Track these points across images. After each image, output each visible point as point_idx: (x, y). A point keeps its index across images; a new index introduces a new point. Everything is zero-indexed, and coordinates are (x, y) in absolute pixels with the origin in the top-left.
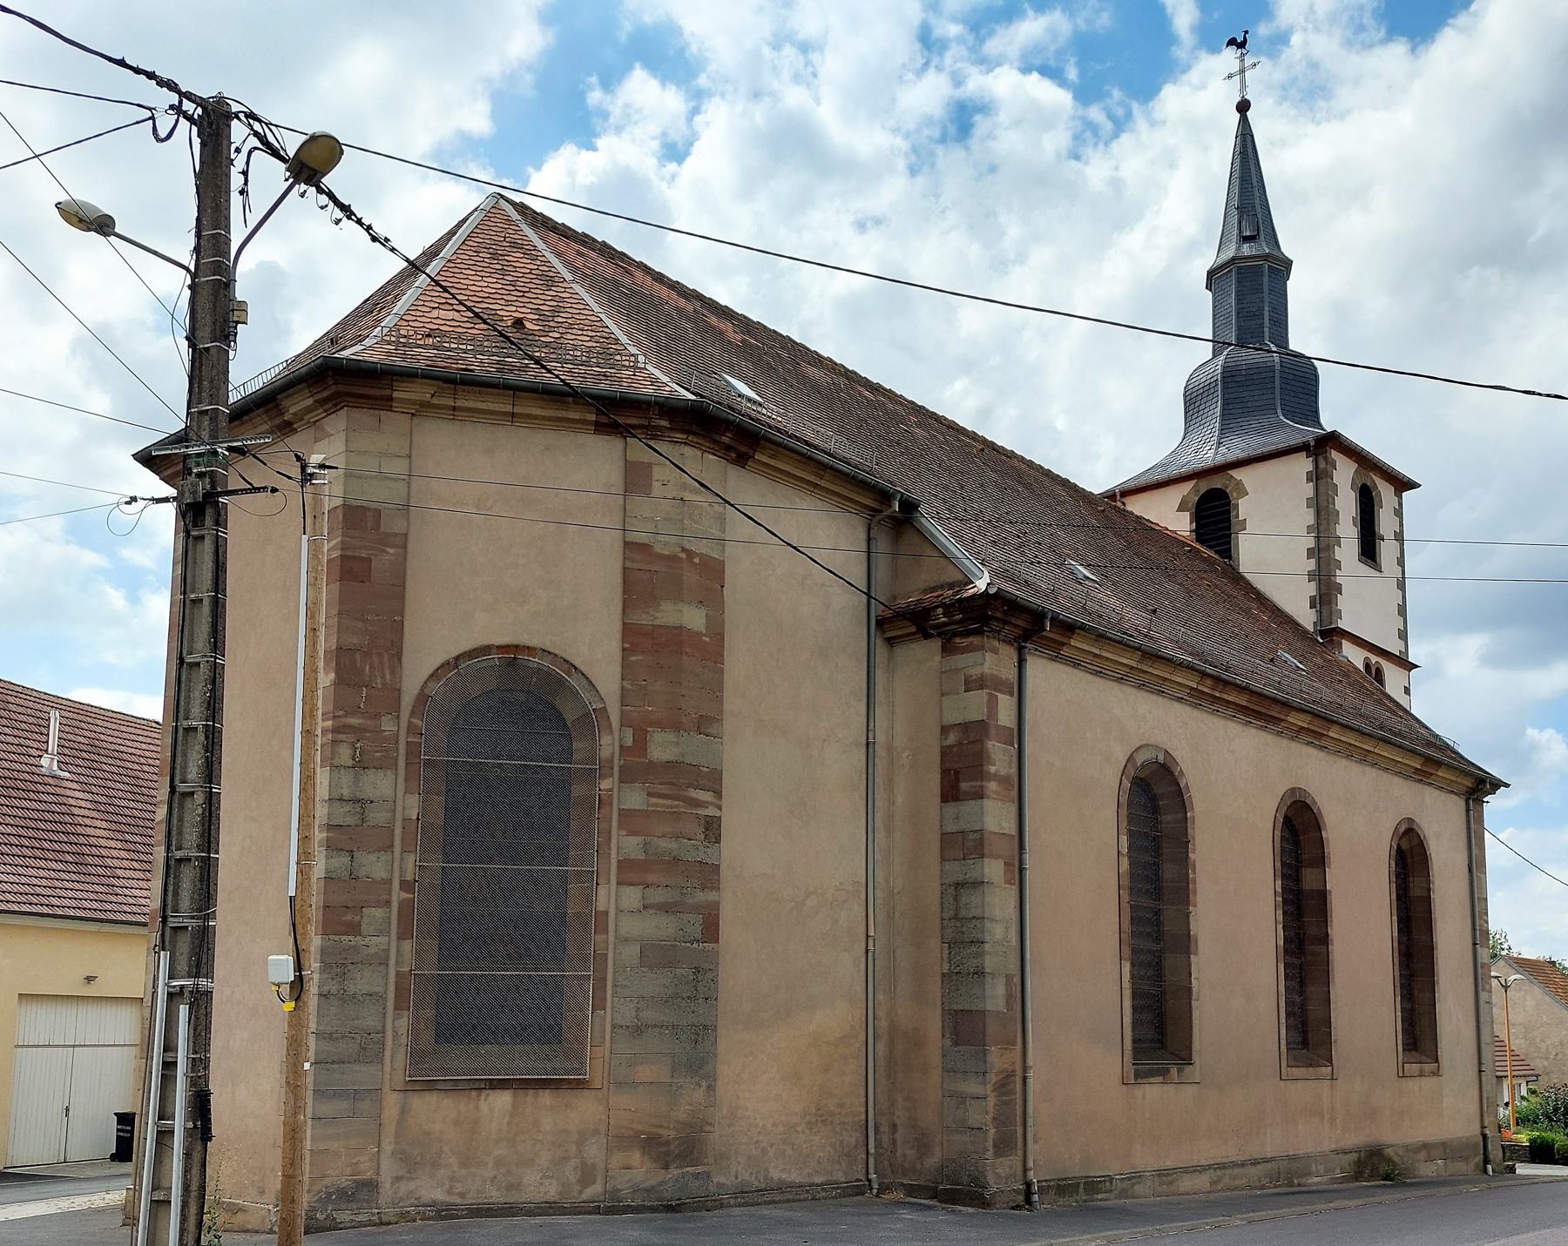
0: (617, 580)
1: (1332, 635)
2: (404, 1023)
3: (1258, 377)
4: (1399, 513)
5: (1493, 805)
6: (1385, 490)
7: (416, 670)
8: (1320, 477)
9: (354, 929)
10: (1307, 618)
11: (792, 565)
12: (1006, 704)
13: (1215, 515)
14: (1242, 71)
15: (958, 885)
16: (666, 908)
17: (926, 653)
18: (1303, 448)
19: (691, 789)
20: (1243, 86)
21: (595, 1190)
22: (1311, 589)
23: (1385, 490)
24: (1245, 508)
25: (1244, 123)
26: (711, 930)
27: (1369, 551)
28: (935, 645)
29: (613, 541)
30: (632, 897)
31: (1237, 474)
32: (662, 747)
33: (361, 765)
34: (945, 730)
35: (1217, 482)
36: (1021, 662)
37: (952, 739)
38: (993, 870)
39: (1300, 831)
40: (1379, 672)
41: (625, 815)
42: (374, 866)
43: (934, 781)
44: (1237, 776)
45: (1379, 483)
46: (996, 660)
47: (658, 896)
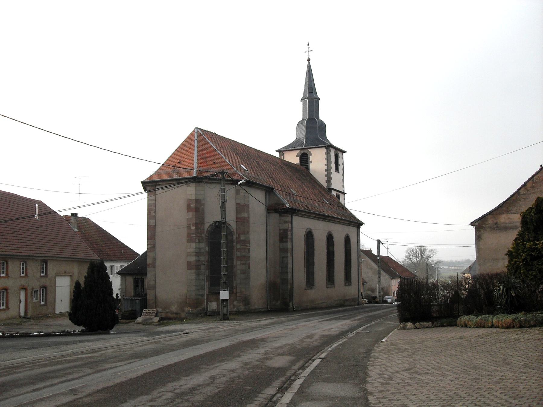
0: (235, 209)
1: (330, 190)
2: (207, 284)
3: (313, 130)
4: (343, 158)
5: (362, 228)
6: (340, 154)
7: (207, 226)
8: (328, 153)
9: (200, 269)
10: (325, 185)
11: (257, 201)
12: (290, 225)
13: (305, 158)
14: (309, 51)
15: (284, 257)
16: (243, 264)
17: (276, 215)
18: (325, 147)
19: (246, 242)
20: (309, 55)
21: (235, 309)
22: (326, 179)
23: (340, 154)
24: (311, 158)
25: (309, 63)
26: (249, 268)
27: (337, 169)
28: (278, 214)
29: (234, 202)
30: (239, 262)
31: (310, 150)
32: (242, 237)
33: (199, 242)
34: (280, 230)
35: (305, 151)
36: (292, 217)
37: (281, 231)
38: (289, 255)
39: (330, 238)
40: (339, 196)
41: (237, 249)
42: (202, 259)
43: (277, 239)
44: (320, 229)
45: (339, 152)
46: (289, 218)
47: (242, 262)
